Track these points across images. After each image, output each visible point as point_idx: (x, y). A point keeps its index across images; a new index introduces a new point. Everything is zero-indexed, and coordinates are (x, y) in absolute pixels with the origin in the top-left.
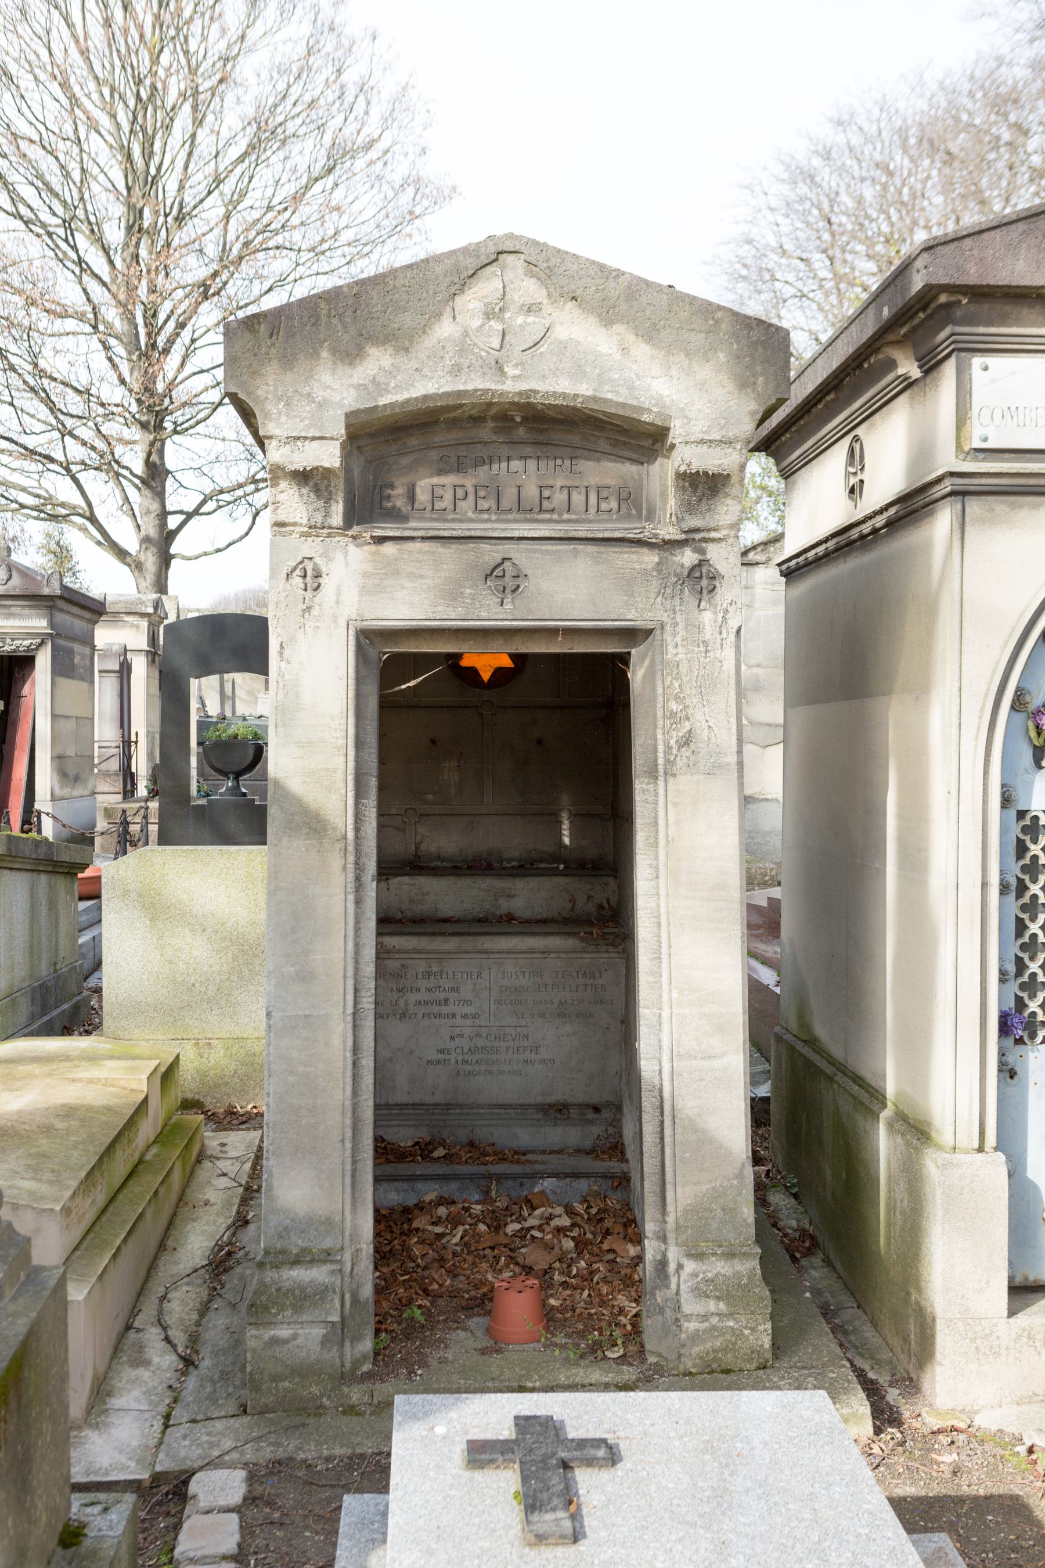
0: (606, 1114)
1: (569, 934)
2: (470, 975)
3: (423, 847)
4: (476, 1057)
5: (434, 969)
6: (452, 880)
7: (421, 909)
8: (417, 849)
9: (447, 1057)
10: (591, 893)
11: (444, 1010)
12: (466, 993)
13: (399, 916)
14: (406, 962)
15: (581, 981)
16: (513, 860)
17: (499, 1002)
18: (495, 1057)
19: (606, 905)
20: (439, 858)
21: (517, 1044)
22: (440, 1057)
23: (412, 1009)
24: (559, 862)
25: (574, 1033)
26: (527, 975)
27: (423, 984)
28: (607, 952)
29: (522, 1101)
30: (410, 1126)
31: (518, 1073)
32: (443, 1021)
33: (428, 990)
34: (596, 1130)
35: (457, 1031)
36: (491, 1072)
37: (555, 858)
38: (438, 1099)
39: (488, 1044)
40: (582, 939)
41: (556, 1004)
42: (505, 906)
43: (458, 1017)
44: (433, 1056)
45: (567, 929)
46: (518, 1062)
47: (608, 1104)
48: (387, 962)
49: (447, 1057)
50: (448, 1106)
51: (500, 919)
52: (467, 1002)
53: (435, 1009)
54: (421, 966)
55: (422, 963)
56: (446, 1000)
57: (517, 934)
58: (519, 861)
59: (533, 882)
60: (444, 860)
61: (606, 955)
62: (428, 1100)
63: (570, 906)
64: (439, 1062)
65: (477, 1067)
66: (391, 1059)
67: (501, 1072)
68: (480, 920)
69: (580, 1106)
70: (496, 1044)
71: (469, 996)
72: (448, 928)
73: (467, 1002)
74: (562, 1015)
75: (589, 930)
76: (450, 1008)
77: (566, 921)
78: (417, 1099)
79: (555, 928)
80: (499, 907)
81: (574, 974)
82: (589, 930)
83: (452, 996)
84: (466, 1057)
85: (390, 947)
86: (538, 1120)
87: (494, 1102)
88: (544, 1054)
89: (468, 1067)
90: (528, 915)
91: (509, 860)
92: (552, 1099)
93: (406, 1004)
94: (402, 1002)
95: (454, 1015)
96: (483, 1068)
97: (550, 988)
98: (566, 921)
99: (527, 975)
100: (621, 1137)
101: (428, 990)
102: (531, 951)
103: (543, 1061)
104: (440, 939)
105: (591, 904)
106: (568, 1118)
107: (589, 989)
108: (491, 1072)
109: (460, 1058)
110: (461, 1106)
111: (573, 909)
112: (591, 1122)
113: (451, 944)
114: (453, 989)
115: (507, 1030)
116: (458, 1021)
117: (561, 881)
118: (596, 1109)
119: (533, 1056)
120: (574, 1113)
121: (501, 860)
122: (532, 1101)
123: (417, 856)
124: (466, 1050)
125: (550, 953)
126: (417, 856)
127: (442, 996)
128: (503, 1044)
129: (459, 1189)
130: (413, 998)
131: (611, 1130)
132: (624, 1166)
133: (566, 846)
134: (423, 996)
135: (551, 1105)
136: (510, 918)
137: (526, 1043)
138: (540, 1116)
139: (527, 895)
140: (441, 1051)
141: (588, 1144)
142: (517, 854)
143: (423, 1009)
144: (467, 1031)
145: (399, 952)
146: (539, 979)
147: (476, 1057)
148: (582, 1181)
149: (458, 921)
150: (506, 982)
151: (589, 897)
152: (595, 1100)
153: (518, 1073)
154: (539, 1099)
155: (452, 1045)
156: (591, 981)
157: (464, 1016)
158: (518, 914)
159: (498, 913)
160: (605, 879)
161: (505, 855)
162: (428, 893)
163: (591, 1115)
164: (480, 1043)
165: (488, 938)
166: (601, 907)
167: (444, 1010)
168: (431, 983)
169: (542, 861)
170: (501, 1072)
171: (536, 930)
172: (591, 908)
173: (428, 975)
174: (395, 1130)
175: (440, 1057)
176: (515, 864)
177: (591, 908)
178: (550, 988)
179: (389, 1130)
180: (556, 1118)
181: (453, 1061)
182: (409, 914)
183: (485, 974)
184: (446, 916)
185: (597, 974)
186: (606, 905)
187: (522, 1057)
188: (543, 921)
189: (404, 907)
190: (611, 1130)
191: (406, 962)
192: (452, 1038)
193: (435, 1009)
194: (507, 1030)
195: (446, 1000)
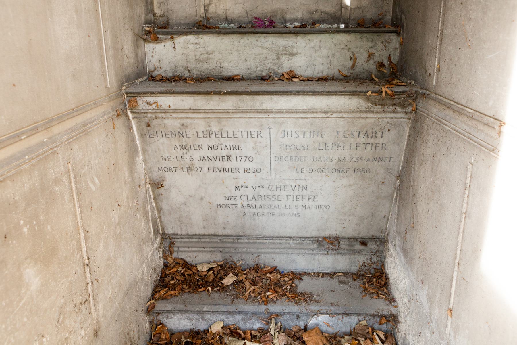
0: (372, 246)
1: (354, 93)
2: (250, 134)
3: (212, 9)
4: (259, 203)
5: (214, 129)
6: (235, 37)
7: (208, 67)
8: (206, 11)
9: (234, 202)
10: (373, 51)
11: (227, 165)
12: (247, 149)
13: (186, 74)
14: (185, 121)
15: (362, 140)
16: (296, 20)
17: (279, 159)
18: (276, 203)
19: (386, 62)
20: (227, 20)
21: (296, 193)
22: (227, 202)
23: (197, 164)
24: (339, 23)
25: (350, 186)
26: (307, 134)
27: (205, 142)
28: (394, 112)
29: (300, 235)
30: (207, 252)
31: (298, 215)
32: (227, 174)
33: (210, 147)
34: (362, 259)
35: (241, 182)
36: (273, 214)
37: (336, 19)
38: (228, 232)
39: (270, 193)
40: (368, 99)
41: (335, 161)
42: (287, 65)
43: (241, 171)
44: (222, 201)
45: (351, 87)
46: (297, 207)
47: (373, 238)
48: (166, 121)
49: (234, 202)
50: (238, 237)
51: (282, 77)
52: (248, 159)
53: (219, 164)
54: (200, 125)
55: (202, 122)
56: (229, 157)
57: (298, 93)
58: (302, 20)
59: (315, 40)
60: (231, 22)
61: (391, 115)
62: (221, 232)
63: (350, 63)
64: (227, 206)
65: (260, 210)
66: (185, 203)
67: (281, 214)
68: (263, 79)
69: (349, 239)
70: (277, 193)
71: (250, 153)
72: (181, 111)
73: (248, 159)
74: (341, 170)
75: (377, 88)
76: (233, 164)
77: (346, 79)
78: (212, 232)
79: (339, 87)
80: (281, 66)
81: (356, 134)
82: (377, 88)
83: (233, 153)
84: (250, 203)
85: (165, 106)
86: (313, 250)
87: (276, 235)
88: (320, 201)
89: (252, 210)
90: (309, 73)
91: (292, 21)
92: (326, 234)
93: (191, 159)
94: (187, 158)
95: (237, 170)
96: (266, 211)
97: (330, 146)
98: (346, 79)
99: (307, 134)
100: (383, 266)
101: (210, 147)
102: (312, 111)
103: (320, 207)
104: (216, 98)
105: (371, 62)
106: (339, 248)
107: (369, 147)
108: (273, 214)
109: (245, 204)
110: (249, 237)
111: (353, 66)
112: (359, 252)
113: (229, 103)
114: (234, 147)
115: (287, 182)
116: (241, 174)
117: (344, 38)
118: (364, 243)
119: (311, 203)
120: (344, 245)
121: (285, 21)
122: (309, 235)
123: (207, 19)
124: (250, 197)
125: (332, 113)
126: (207, 19)
127: (225, 153)
128: (284, 194)
129: (243, 320)
130: (197, 154)
131: (374, 259)
132: (394, 311)
133: (346, 7)
134: (206, 152)
135: (324, 238)
136: (292, 76)
137: (305, 193)
138: (315, 246)
139: (310, 54)
140: (229, 198)
141: (354, 269)
142: (299, 15)
143: (207, 164)
144: (251, 183)
145: (175, 111)
146: (319, 138)
147: (259, 203)
148: (353, 317)
149: (241, 79)
150: (286, 141)
151: (370, 55)
152: (363, 233)
153: (298, 215)
154: (315, 234)
155: (238, 193)
156: (372, 141)
157: (247, 170)
158: (299, 72)
159: (280, 71)
160: (387, 36)
161: (288, 16)
162: (213, 52)
163: (358, 246)
164: (263, 192)
165: (267, 97)
166: (381, 65)
167: (227, 165)
168: (213, 141)
169: (322, 22)
170: (281, 214)
171: (318, 89)
172: (371, 66)
173: (209, 134)
174: (195, 254)
175: (227, 202)
176: (297, 24)
177: (371, 66)
178: (330, 146)
179: (190, 254)
180: (328, 248)
181: (239, 206)
182: (196, 73)
183: (265, 133)
184: (230, 74)
185: (379, 134)
186: (386, 62)
187: (300, 203)
188: (324, 79)
189: (191, 66)
190: (374, 259)
191: (185, 121)
192: (237, 188)
193: (219, 164)
194: (287, 182)
195: (229, 157)
